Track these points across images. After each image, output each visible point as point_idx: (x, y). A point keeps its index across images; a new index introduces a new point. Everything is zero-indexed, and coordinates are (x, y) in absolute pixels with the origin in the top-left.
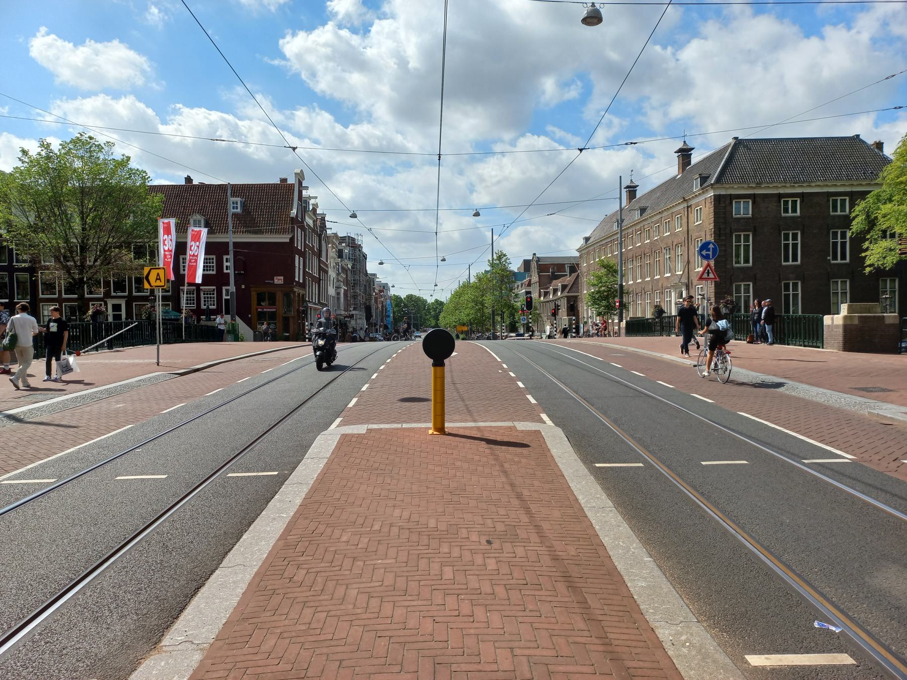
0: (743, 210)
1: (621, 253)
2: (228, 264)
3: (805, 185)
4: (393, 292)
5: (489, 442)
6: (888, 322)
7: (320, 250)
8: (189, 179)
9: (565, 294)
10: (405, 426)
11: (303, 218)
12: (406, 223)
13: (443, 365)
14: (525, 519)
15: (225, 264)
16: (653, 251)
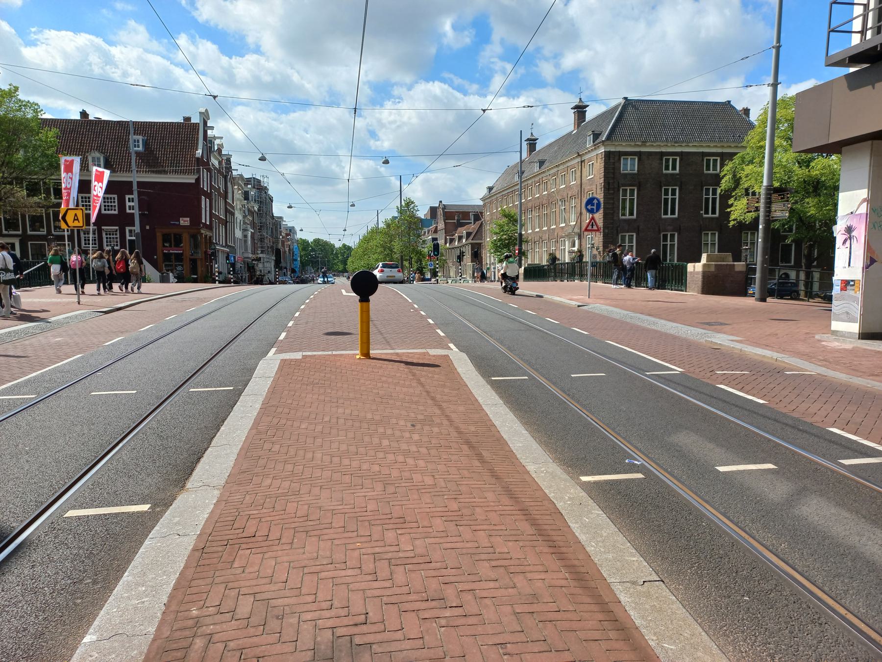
0: (630, 166)
1: (521, 203)
2: (132, 205)
3: (684, 144)
4: (299, 235)
5: (407, 363)
6: (737, 269)
7: (226, 192)
8: (84, 114)
9: (470, 241)
10: (334, 353)
11: (209, 159)
12: (306, 165)
13: (368, 301)
14: (438, 412)
15: (128, 204)
16: (549, 202)
